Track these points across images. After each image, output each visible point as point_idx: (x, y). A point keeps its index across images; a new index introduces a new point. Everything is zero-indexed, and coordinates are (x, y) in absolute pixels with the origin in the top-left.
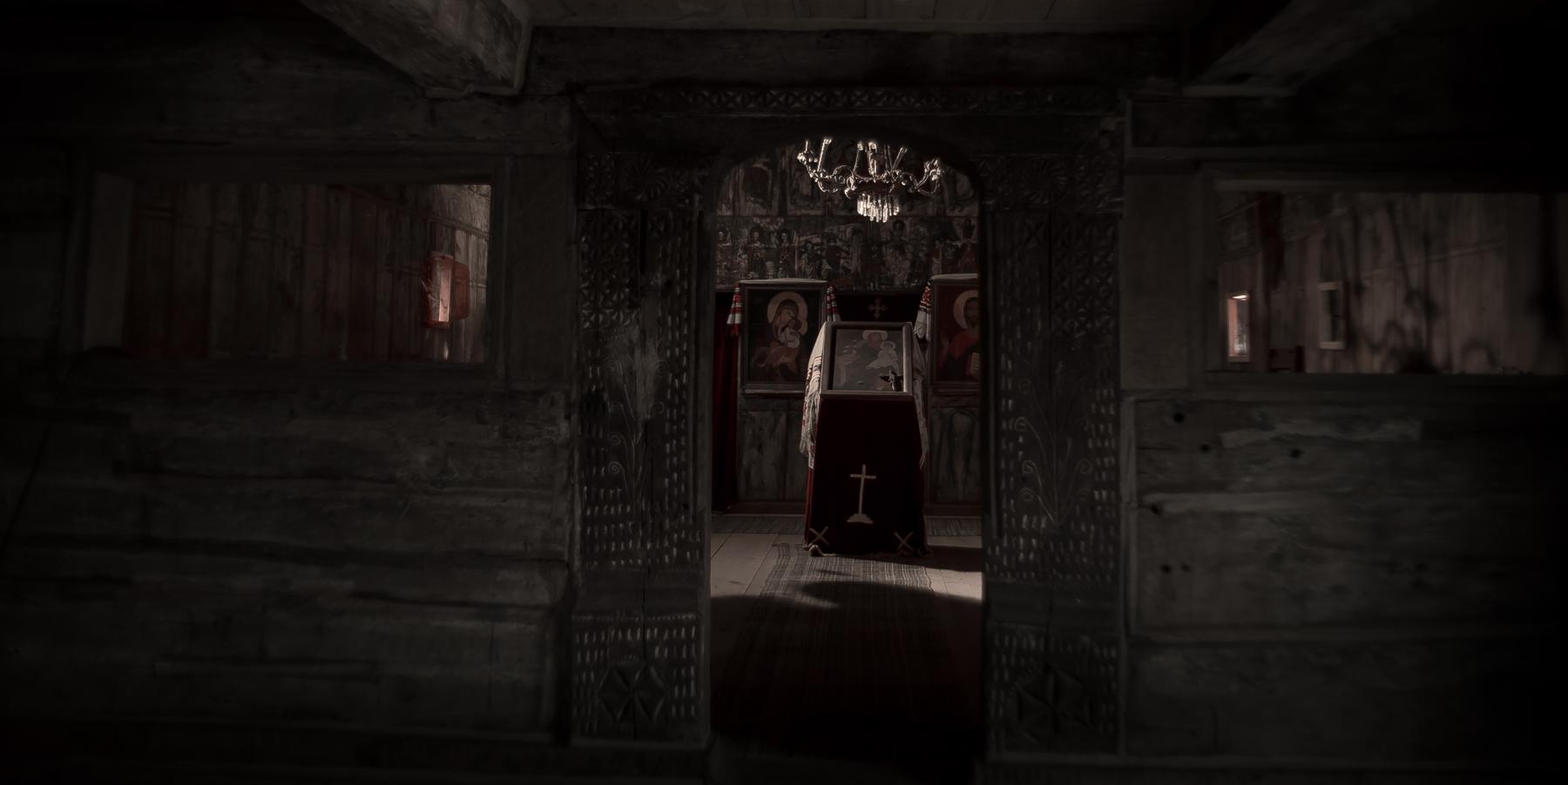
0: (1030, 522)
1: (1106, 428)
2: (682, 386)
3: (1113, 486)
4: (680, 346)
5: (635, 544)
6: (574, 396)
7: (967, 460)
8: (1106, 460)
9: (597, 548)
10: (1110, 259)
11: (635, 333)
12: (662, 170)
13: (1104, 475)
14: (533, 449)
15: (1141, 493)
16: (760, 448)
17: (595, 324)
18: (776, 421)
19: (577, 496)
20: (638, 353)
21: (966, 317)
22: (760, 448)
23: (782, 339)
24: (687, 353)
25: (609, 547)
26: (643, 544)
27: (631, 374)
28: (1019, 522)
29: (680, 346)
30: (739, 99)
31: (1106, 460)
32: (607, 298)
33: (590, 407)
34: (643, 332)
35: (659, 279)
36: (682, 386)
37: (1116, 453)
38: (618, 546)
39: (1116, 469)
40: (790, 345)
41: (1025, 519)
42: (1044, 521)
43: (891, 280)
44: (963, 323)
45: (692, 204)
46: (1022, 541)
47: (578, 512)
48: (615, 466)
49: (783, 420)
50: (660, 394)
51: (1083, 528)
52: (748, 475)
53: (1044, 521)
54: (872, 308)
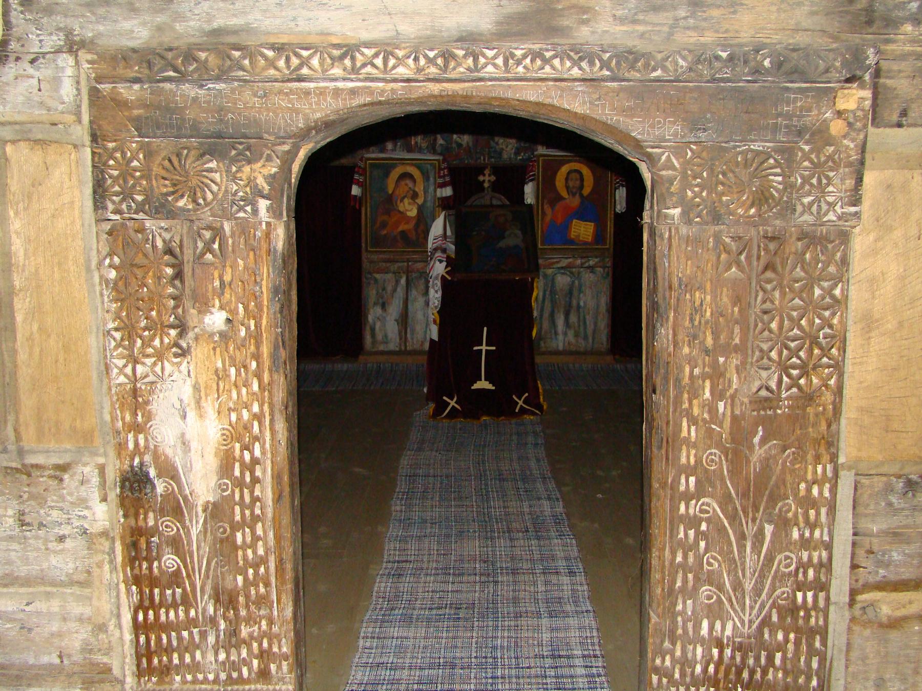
0: (711, 628)
1: (818, 514)
2: (255, 461)
3: (821, 586)
4: (247, 406)
5: (203, 655)
6: (112, 475)
7: (567, 315)
8: (815, 555)
9: (156, 661)
10: (837, 292)
11: (187, 391)
12: (213, 165)
13: (811, 572)
14: (62, 539)
15: (853, 593)
16: (383, 306)
17: (134, 379)
18: (397, 282)
19: (123, 596)
20: (191, 414)
21: (567, 187)
22: (383, 306)
23: (401, 209)
24: (259, 417)
25: (170, 660)
26: (216, 654)
27: (185, 444)
28: (697, 627)
29: (247, 406)
30: (315, 62)
31: (815, 555)
32: (147, 343)
33: (134, 486)
34: (196, 388)
35: (216, 319)
36: (255, 461)
37: (829, 547)
38: (181, 658)
39: (826, 566)
40: (409, 214)
41: (705, 624)
42: (729, 626)
43: (500, 153)
44: (564, 193)
45: (255, 212)
46: (699, 650)
47: (127, 618)
48: (170, 561)
49: (403, 281)
50: (225, 468)
51: (780, 636)
52: (373, 330)
53: (729, 626)
54: (481, 178)
